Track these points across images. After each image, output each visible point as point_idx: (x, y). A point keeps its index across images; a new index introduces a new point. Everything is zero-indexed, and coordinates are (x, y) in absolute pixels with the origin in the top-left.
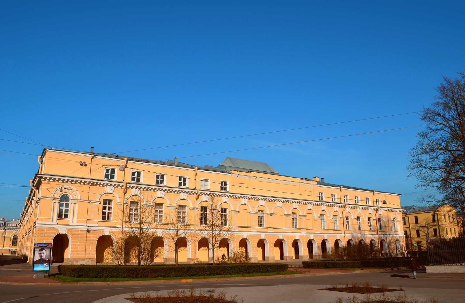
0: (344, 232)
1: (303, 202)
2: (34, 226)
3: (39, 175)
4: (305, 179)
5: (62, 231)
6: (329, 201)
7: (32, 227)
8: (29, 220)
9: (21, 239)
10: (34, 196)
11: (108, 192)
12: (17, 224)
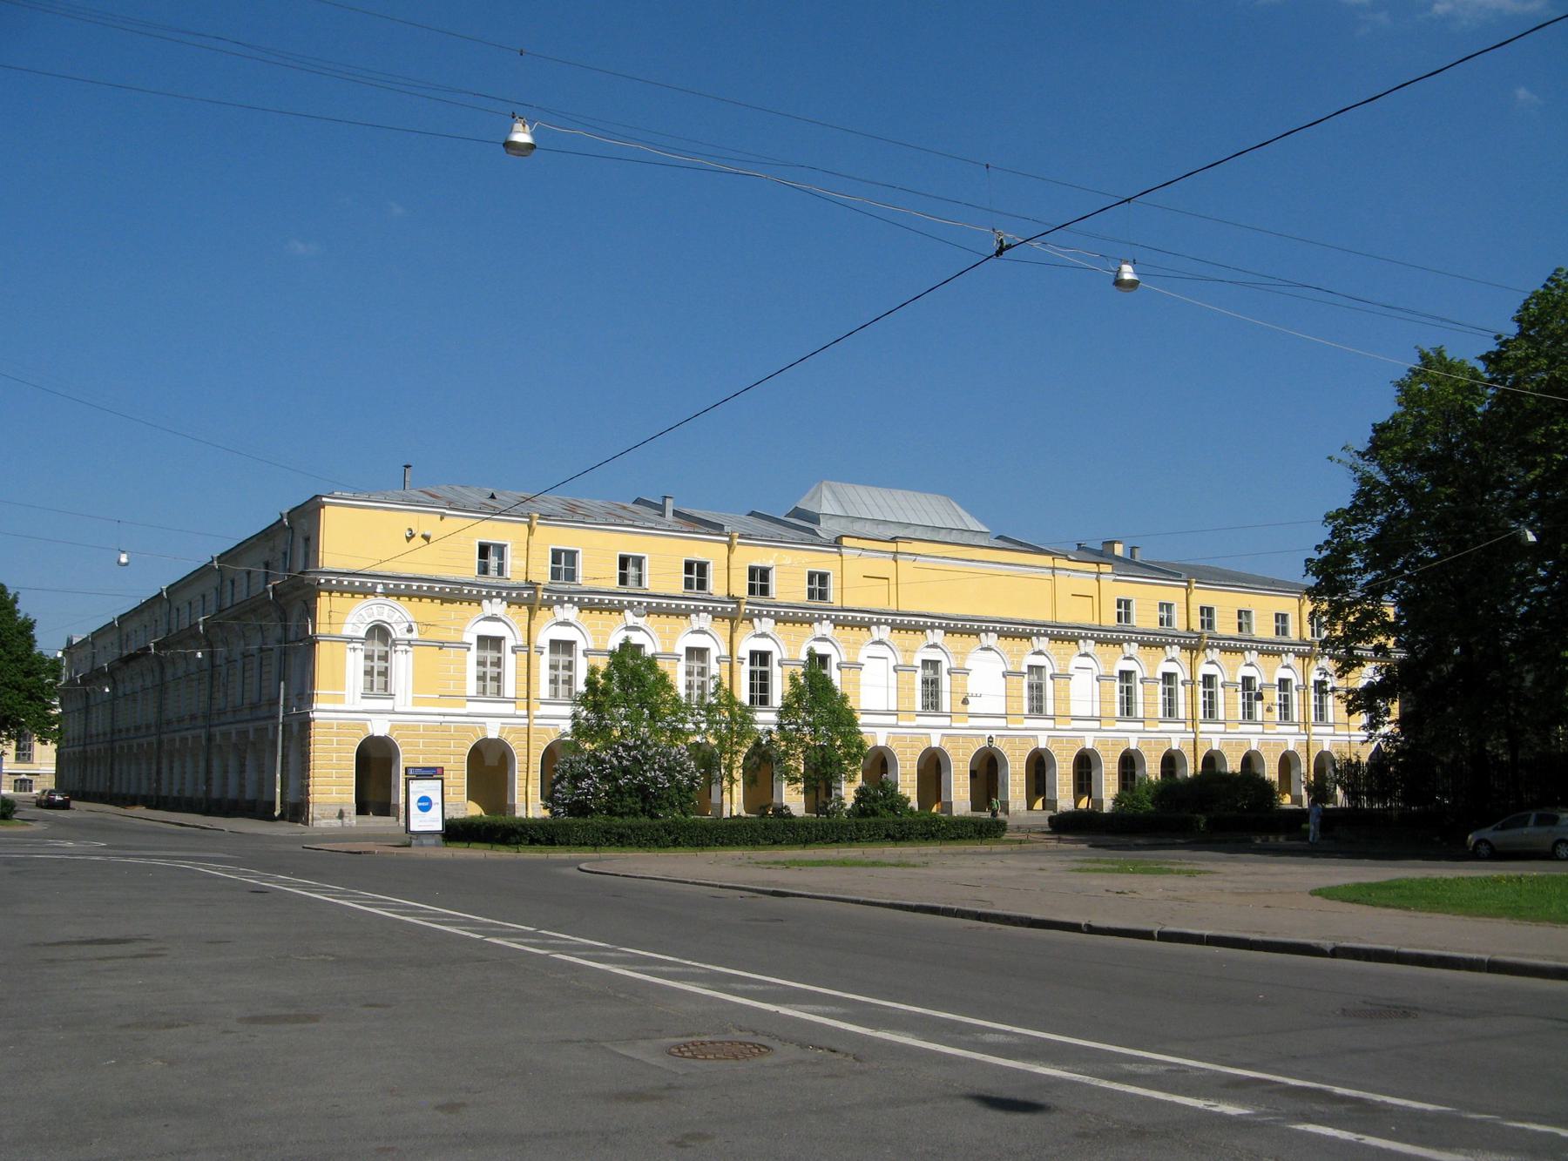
0: (528, 709)
1: (1064, 634)
5: (379, 728)
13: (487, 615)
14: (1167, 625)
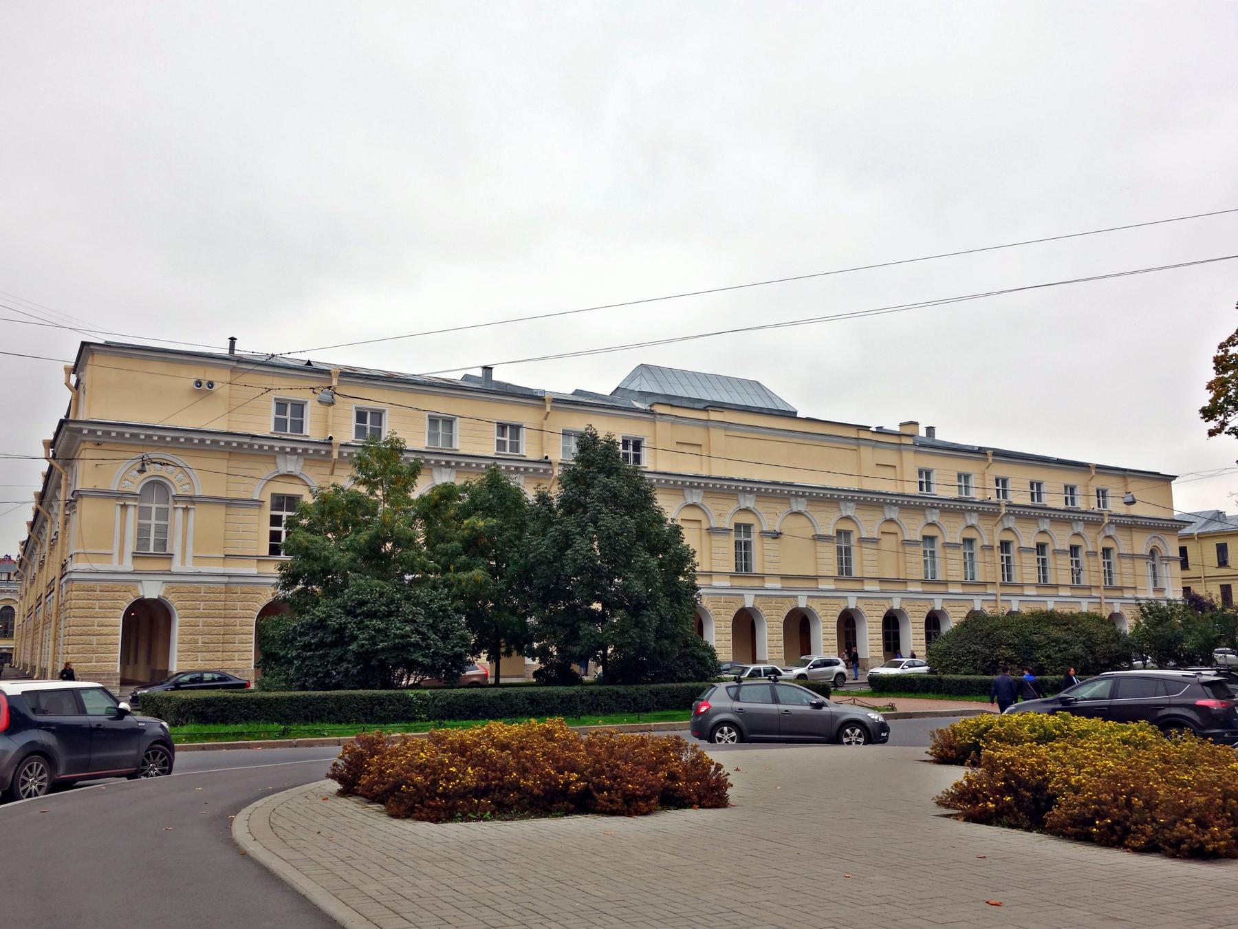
2: (61, 579)
3: (71, 425)
4: (877, 428)
5: (151, 590)
6: (1058, 507)
7: (57, 580)
8: (46, 560)
9: (24, 616)
10: (58, 487)
11: (286, 473)
12: (9, 574)
13: (794, 511)
14: (1103, 507)
